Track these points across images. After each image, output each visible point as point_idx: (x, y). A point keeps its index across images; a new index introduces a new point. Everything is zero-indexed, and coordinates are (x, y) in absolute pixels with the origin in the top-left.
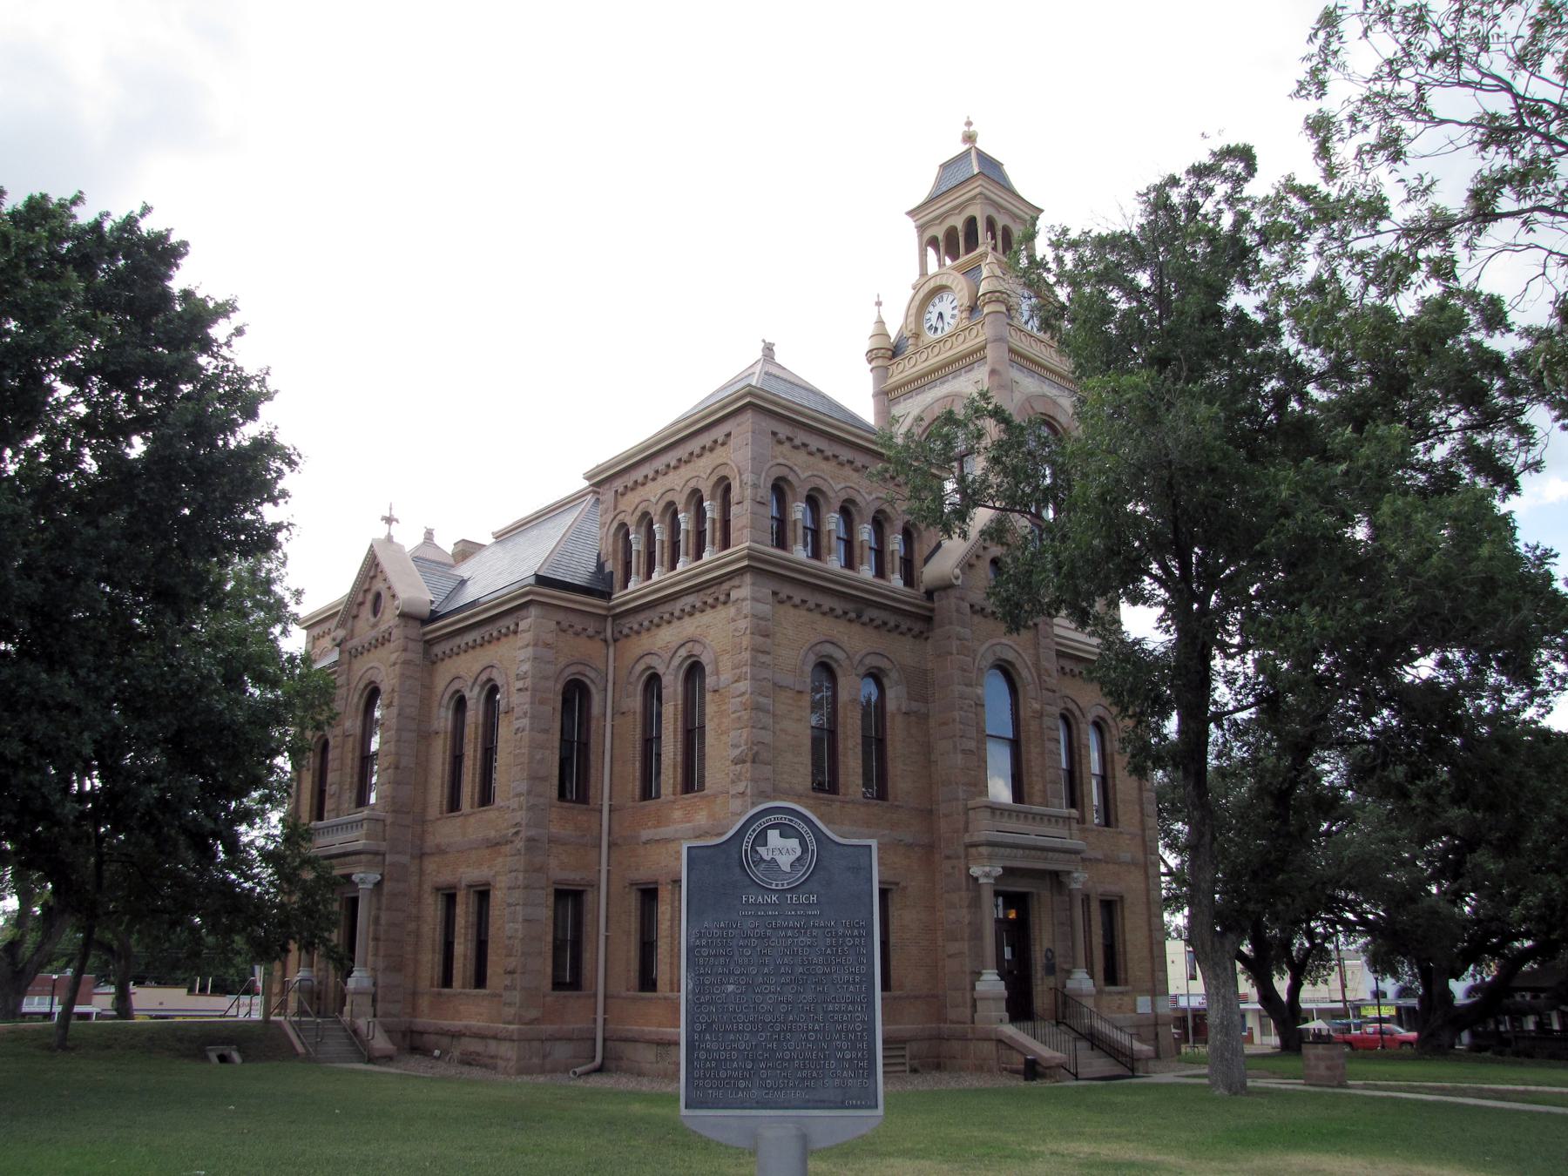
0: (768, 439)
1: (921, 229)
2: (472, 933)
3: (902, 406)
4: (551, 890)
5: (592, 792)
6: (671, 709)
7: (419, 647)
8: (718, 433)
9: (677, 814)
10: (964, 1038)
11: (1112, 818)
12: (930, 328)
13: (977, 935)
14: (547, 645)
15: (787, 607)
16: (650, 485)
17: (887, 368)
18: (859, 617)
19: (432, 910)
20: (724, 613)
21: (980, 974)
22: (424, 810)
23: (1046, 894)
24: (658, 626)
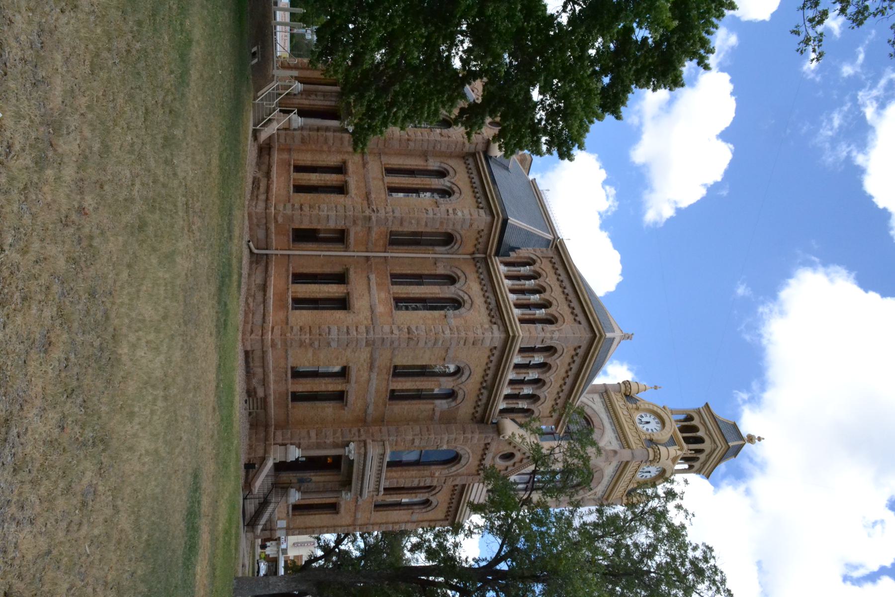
0: (576, 345)
1: (699, 412)
2: (322, 183)
3: (599, 400)
4: (344, 228)
5: (395, 247)
6: (437, 291)
7: (472, 150)
8: (581, 317)
9: (383, 295)
10: (266, 439)
11: (378, 509)
12: (642, 417)
13: (318, 446)
14: (471, 225)
15: (489, 353)
16: (555, 277)
17: (620, 392)
18: (484, 388)
19: (333, 160)
20: (485, 319)
21: (299, 448)
22: (386, 154)
23: (340, 478)
24: (480, 283)
